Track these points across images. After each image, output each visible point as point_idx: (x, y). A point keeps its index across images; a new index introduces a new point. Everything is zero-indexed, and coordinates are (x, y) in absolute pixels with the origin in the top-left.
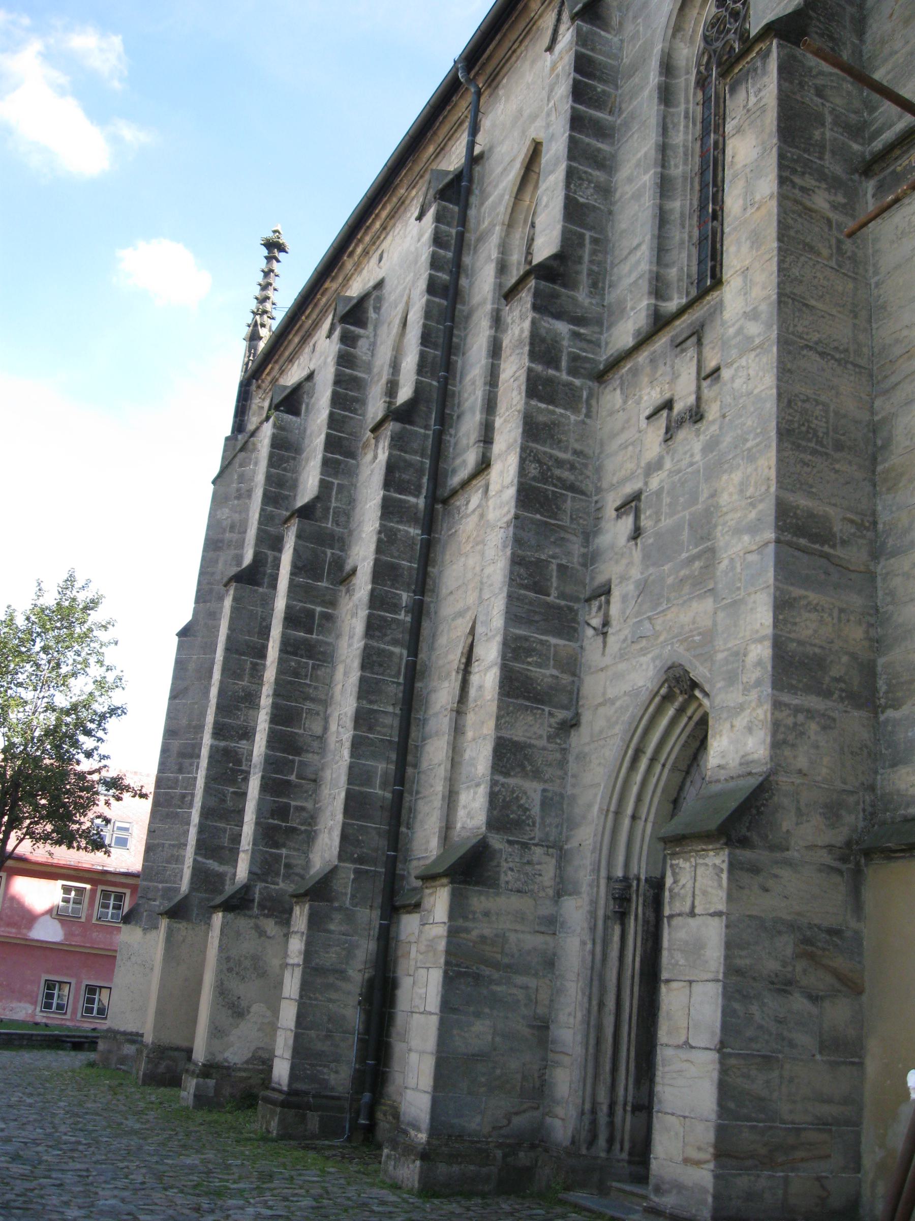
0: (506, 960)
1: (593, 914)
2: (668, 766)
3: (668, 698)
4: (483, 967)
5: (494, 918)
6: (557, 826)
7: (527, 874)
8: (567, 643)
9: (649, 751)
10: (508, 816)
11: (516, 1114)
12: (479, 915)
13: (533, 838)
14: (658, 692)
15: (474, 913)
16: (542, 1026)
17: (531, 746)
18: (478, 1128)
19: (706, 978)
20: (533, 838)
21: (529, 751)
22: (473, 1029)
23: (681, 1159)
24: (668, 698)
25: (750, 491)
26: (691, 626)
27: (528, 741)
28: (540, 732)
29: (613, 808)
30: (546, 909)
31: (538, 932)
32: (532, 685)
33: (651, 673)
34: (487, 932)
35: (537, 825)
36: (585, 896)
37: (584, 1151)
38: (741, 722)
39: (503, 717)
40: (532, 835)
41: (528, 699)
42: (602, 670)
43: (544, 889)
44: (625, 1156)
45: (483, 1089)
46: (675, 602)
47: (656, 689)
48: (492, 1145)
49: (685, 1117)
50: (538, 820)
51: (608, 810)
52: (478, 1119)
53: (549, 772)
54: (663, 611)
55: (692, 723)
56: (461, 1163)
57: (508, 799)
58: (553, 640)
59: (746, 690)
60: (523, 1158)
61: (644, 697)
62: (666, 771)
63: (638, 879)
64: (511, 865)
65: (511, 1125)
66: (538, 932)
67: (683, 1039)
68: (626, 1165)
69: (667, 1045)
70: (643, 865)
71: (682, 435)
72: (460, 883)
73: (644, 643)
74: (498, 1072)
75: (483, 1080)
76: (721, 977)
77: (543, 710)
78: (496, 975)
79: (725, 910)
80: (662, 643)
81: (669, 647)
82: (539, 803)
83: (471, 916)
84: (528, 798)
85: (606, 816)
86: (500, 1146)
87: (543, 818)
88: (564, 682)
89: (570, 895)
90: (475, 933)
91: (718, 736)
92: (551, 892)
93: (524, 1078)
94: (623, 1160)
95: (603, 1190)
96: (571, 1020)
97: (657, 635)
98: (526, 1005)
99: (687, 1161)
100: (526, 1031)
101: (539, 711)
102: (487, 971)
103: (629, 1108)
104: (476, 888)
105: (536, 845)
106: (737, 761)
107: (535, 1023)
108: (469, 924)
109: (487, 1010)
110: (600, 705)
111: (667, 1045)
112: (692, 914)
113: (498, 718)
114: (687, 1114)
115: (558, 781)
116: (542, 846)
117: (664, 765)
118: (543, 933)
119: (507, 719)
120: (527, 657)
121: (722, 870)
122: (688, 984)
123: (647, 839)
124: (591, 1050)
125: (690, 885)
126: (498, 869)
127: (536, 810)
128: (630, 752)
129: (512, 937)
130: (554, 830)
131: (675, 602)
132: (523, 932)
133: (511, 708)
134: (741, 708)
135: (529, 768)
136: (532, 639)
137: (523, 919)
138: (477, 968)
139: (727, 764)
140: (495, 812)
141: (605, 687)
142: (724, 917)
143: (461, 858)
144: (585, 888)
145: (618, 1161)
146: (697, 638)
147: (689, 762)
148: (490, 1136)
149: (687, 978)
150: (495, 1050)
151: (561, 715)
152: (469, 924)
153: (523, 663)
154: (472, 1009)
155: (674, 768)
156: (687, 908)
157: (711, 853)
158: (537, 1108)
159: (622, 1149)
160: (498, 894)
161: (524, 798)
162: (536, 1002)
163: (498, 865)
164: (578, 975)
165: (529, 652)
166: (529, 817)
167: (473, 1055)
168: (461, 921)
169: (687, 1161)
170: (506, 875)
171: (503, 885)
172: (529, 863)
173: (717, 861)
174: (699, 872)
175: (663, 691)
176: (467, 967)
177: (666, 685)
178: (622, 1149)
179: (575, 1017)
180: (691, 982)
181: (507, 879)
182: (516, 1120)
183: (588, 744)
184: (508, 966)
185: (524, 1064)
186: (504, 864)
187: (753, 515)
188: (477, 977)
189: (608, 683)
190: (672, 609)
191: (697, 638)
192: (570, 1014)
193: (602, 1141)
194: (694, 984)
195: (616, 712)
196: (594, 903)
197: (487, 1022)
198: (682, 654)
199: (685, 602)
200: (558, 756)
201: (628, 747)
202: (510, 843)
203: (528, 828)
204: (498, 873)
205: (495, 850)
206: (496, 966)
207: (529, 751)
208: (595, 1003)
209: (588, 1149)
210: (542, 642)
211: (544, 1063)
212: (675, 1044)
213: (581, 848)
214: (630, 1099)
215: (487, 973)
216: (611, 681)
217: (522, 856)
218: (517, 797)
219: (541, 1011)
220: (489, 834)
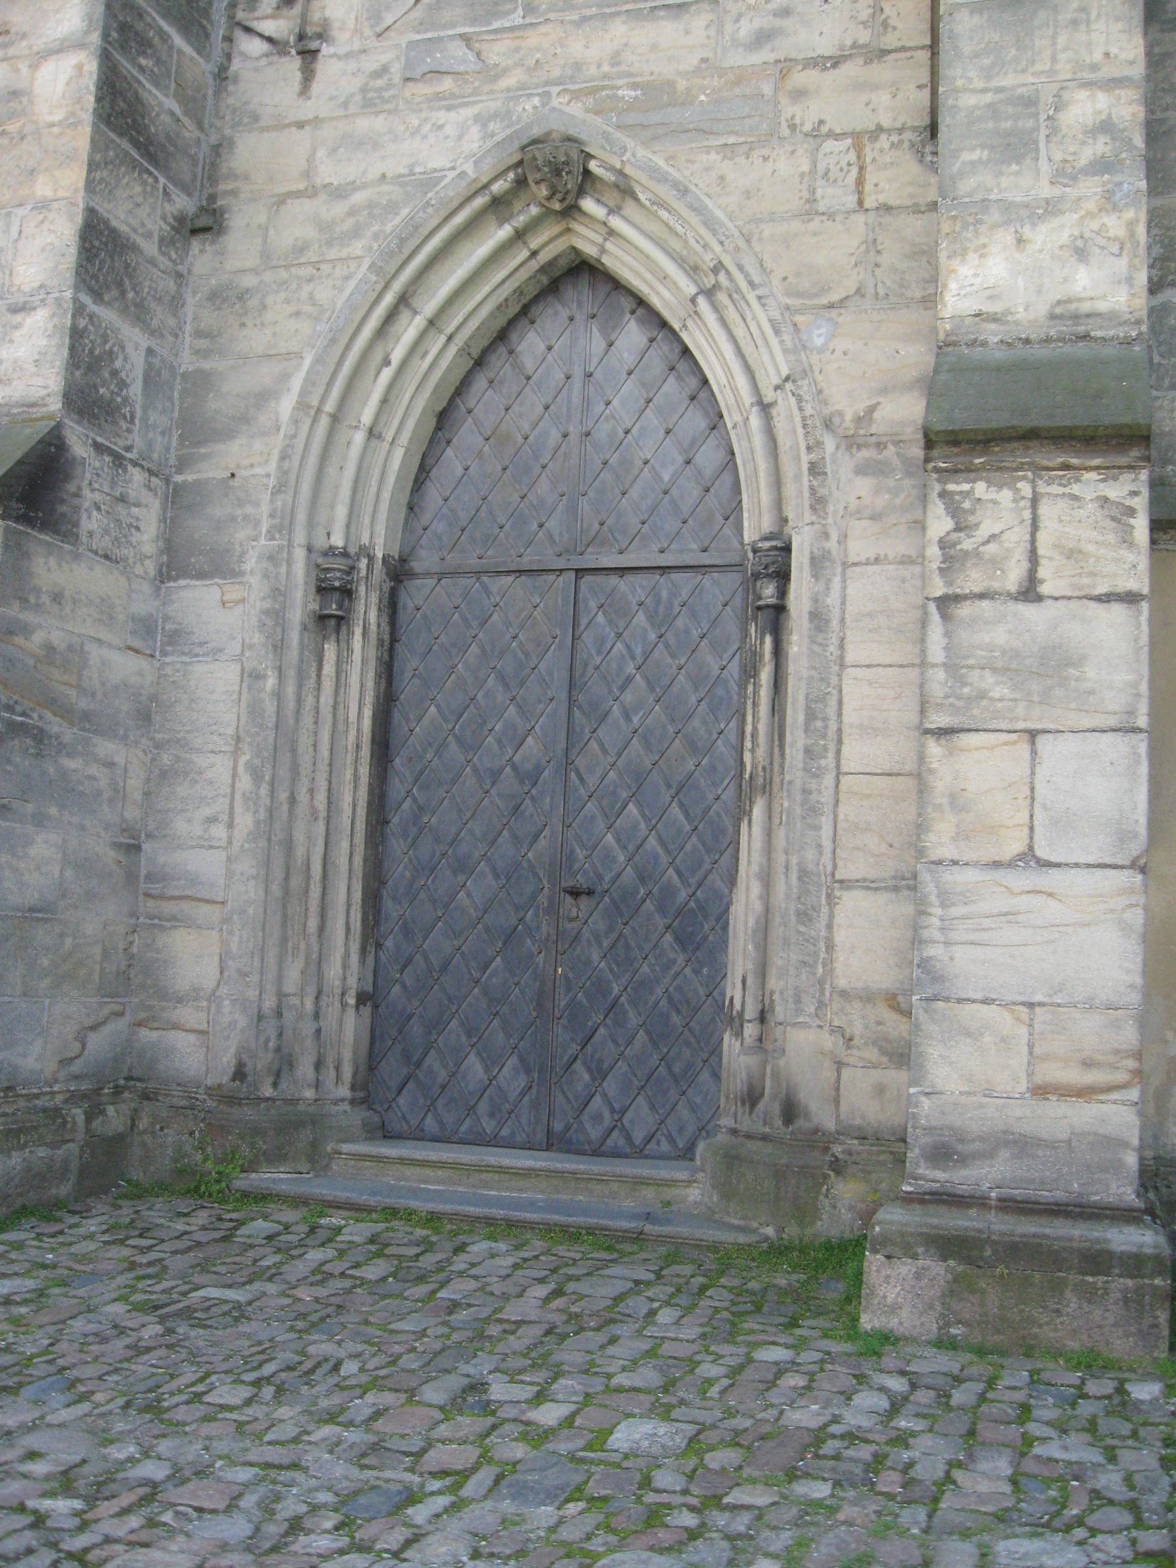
0: (83, 704)
1: (277, 615)
2: (460, 340)
3: (499, 206)
4: (48, 715)
5: (68, 609)
6: (163, 433)
7: (118, 522)
8: (195, 55)
9: (429, 306)
10: (95, 387)
11: (93, 1028)
12: (45, 599)
13: (128, 449)
14: (486, 186)
15: (38, 591)
16: (129, 846)
17: (135, 248)
18: (38, 1066)
19: (1088, 726)
20: (128, 449)
21: (131, 258)
22: (33, 851)
23: (1023, 1086)
24: (499, 206)
26: (606, 68)
27: (133, 236)
28: (150, 225)
29: (330, 407)
30: (143, 605)
31: (130, 648)
32: (143, 117)
33: (473, 142)
34: (57, 638)
35: (137, 421)
36: (254, 580)
37: (268, 1091)
39: (98, 166)
40: (129, 443)
41: (136, 144)
42: (300, 125)
43: (143, 558)
44: (344, 1091)
45: (45, 983)
46: (551, 16)
47: (485, 180)
48: (59, 1098)
49: (1031, 1005)
50: (139, 413)
51: (319, 410)
52: (37, 1048)
53: (160, 315)
54: (512, 29)
55: (534, 265)
56: (25, 1146)
57: (97, 352)
58: (178, 41)
59: (1065, 174)
60: (114, 1119)
61: (450, 189)
62: (452, 350)
63: (371, 559)
64: (97, 496)
65: (86, 1052)
66: (130, 648)
67: (1016, 846)
68: (347, 1107)
69: (955, 863)
70: (381, 529)
72: (18, 519)
73: (447, 84)
74: (68, 941)
75: (46, 963)
76: (1142, 721)
77: (156, 180)
78: (69, 734)
79: (1146, 591)
80: (508, 90)
81: (536, 101)
82: (141, 377)
83: (33, 600)
84: (126, 359)
85: (315, 420)
86: (74, 1098)
87: (145, 409)
88: (187, 135)
89: (201, 575)
90: (38, 637)
91: (972, 257)
92: (151, 567)
93: (106, 954)
94: (343, 1100)
95: (317, 1159)
96: (219, 832)
97: (491, 74)
98: (110, 801)
99: (1041, 1091)
100: (110, 856)
101: (151, 180)
102: (55, 725)
103: (352, 1001)
104: (43, 537)
105: (135, 464)
106: (1042, 310)
107: (122, 840)
108: (27, 617)
109: (53, 811)
110: (297, 194)
111: (955, 863)
112: (1030, 592)
113: (92, 166)
114: (1039, 998)
115: (170, 338)
116: (142, 467)
117: (450, 338)
118: (137, 651)
119: (105, 174)
120: (139, 53)
121: (1131, 511)
122: (1026, 737)
123: (391, 479)
124: (276, 890)
125: (1017, 537)
126: (76, 501)
127: (136, 390)
128: (389, 299)
129: (95, 653)
130: (159, 439)
131: (551, 16)
132: (110, 646)
133: (111, 153)
134: (1051, 208)
135: (131, 295)
136: (149, 20)
137: (111, 618)
138: (41, 717)
139: (1008, 312)
140: (78, 373)
141: (311, 159)
142: (1145, 606)
143: (20, 462)
144: (251, 563)
145: (336, 1102)
146: (629, 94)
147: (486, 343)
148: (56, 1081)
149: (1021, 725)
150: (64, 896)
151: (183, 203)
152: (27, 617)
153: (134, 62)
154: (30, 807)
155: (464, 351)
156: (1014, 577)
157: (1093, 476)
158: (122, 1014)
159: (338, 1078)
160: (76, 557)
161: (121, 357)
162: (125, 796)
163: (77, 495)
164: (238, 739)
165: (144, 45)
166: (126, 400)
167: (32, 910)
168: (16, 605)
169: (1041, 1091)
170: (89, 517)
171: (84, 539)
172: (122, 499)
173: (1116, 491)
174: (1044, 509)
175: (498, 187)
176: (23, 714)
177: (511, 176)
178: (338, 1078)
179: (230, 825)
180: (1033, 735)
181: (90, 527)
182: (96, 1041)
183: (255, 271)
184: (86, 716)
185: (105, 925)
186: (86, 492)
188: (40, 736)
189: (321, 154)
190: (543, 29)
191: (629, 94)
192: (212, 820)
193: (305, 1069)
194: (1041, 740)
195: (352, 213)
196: (279, 594)
197: (54, 837)
199: (585, 19)
200: (171, 285)
201: (386, 287)
202: (97, 446)
203: (124, 425)
204: (76, 510)
205: (74, 459)
206: (66, 713)
207: (131, 258)
208: (283, 796)
209: (275, 1085)
210: (161, 33)
211: (133, 921)
212: (984, 860)
213: (236, 482)
214: (352, 982)
215: (56, 729)
216: (334, 150)
217: (113, 484)
218: (111, 352)
219: (132, 813)
220: (66, 421)
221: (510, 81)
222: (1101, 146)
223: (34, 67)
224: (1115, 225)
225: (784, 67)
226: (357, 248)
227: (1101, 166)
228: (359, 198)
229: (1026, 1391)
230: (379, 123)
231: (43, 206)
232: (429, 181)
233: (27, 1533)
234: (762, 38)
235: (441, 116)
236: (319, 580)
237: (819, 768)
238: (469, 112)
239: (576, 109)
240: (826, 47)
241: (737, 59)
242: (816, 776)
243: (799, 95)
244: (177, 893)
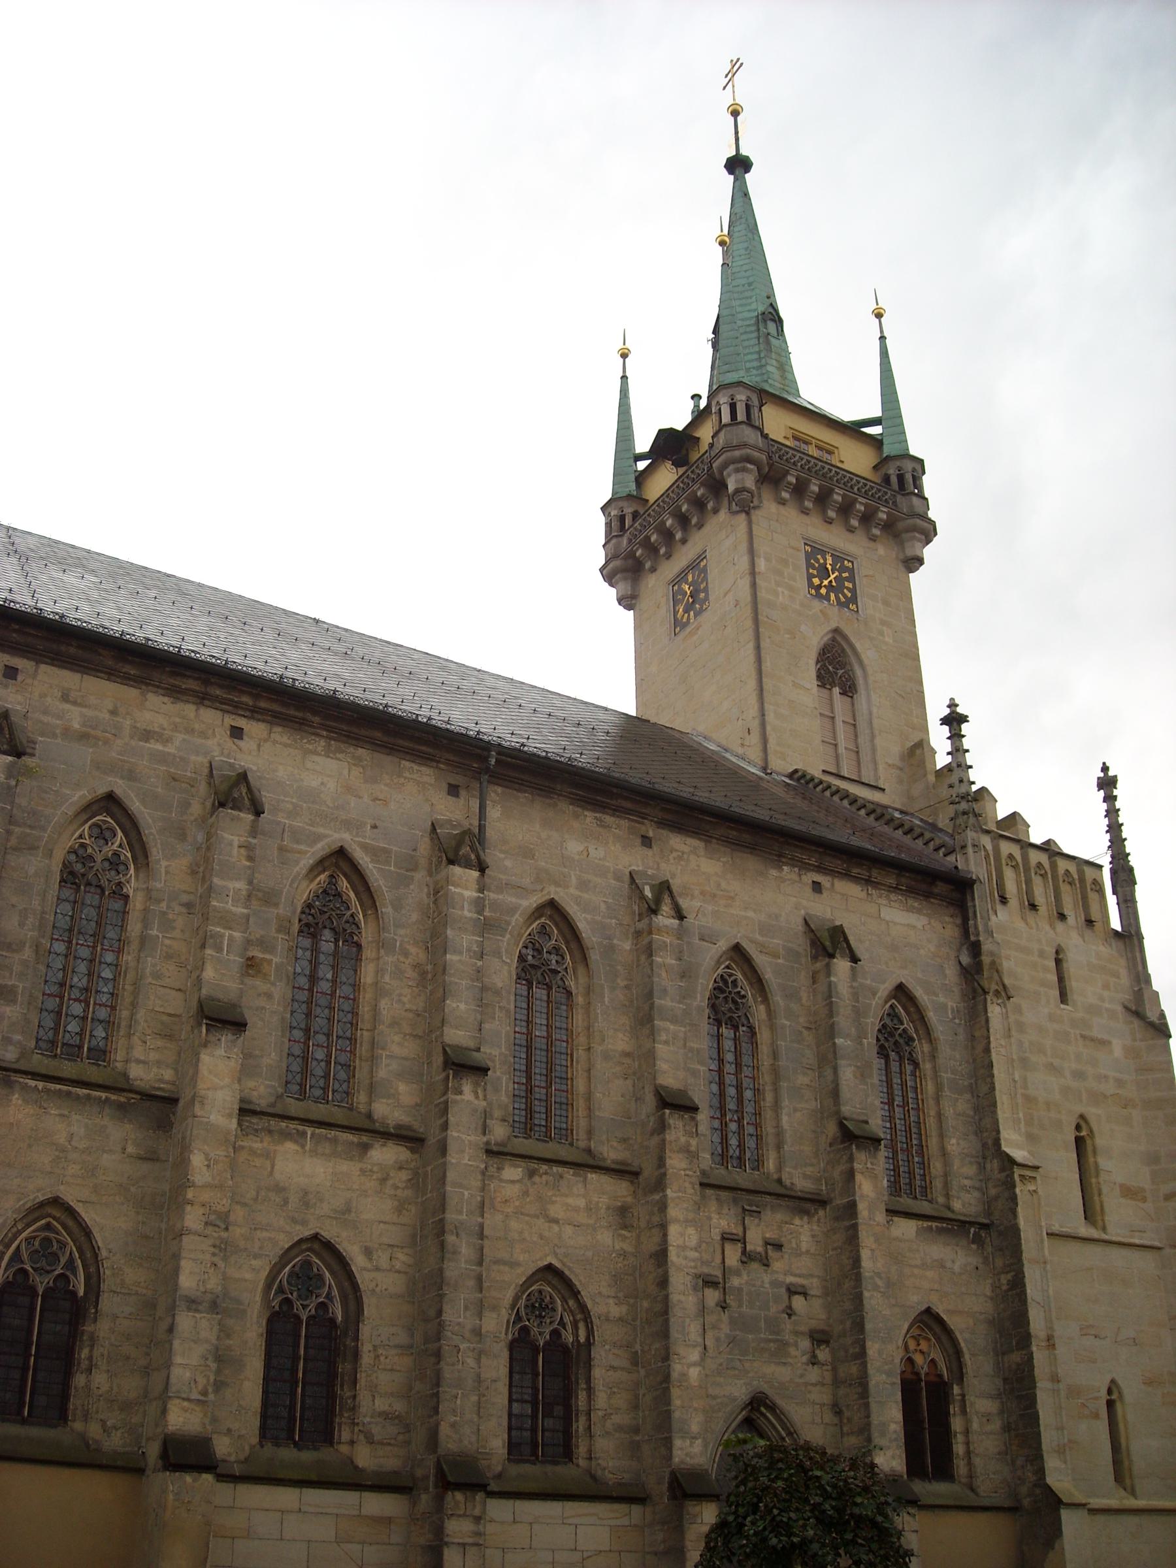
25: (884, 1356)
38: (889, 1453)
71: (755, 1266)
73: (737, 1372)
134: (889, 1448)
187: (886, 1367)
198: (766, 1388)
221: (750, 1375)
222: (894, 1436)
223: (688, 1368)
224: (898, 1452)
225: (806, 1384)
226: (720, 1414)
227: (896, 1440)
228: (719, 1400)
229: (582, 1144)
230: (722, 1380)
231: (696, 1409)
232: (735, 1400)
233: (199, 1114)
234: (801, 1376)
235: (738, 1382)
236: (242, 1100)
237: (222, 1243)
238: (742, 1381)
239: (765, 1386)
240: (814, 1381)
241: (797, 1380)
242: (308, 925)
243: (810, 1392)
244: (755, 738)
